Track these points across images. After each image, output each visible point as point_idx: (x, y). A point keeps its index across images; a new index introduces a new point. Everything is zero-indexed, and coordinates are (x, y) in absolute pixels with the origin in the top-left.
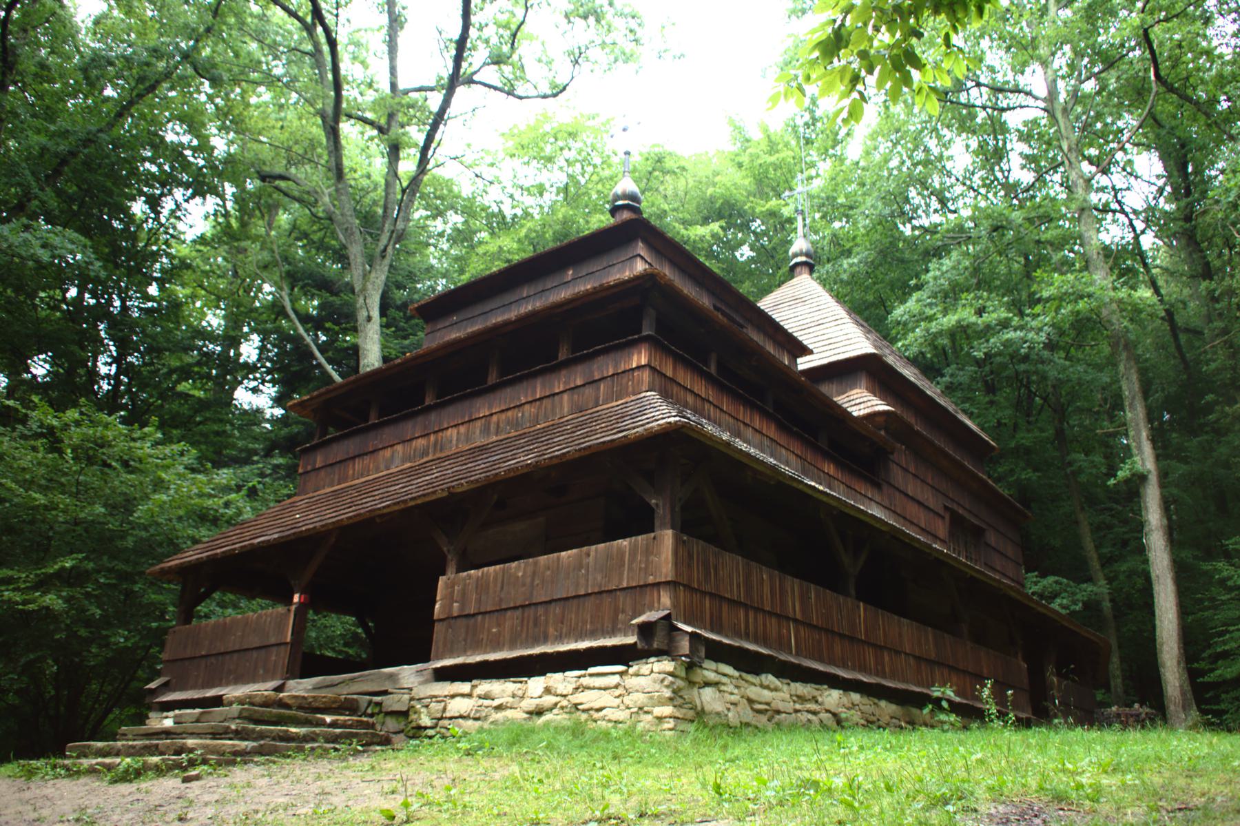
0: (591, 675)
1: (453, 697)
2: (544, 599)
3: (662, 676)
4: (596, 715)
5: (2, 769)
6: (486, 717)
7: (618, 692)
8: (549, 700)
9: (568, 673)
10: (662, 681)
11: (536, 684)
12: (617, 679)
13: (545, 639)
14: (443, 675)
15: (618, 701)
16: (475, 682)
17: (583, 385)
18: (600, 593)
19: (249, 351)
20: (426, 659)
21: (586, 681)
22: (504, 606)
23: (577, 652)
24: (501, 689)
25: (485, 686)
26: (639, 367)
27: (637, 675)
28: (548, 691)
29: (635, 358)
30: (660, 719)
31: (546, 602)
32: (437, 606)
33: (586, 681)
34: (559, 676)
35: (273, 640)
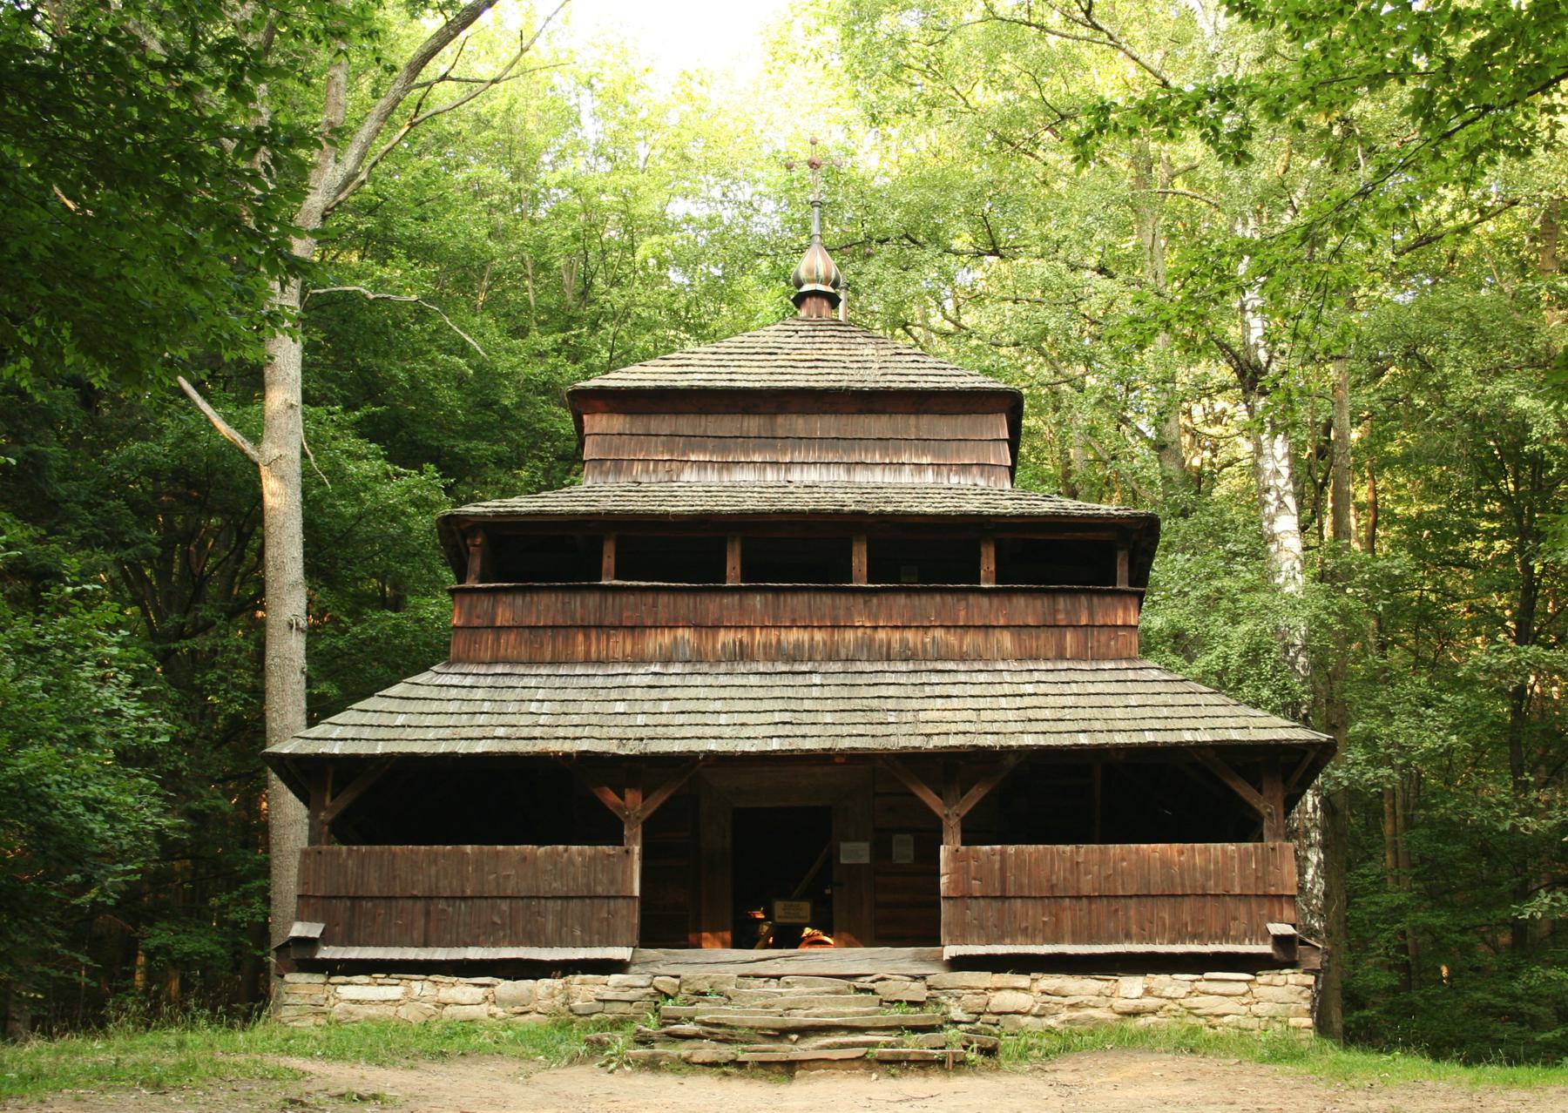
0: (475, 985)
3: (1300, 988)
4: (1216, 1021)
5: (8, 1053)
7: (1245, 1000)
8: (1150, 1002)
10: (1300, 993)
11: (1131, 987)
12: (1243, 987)
14: (959, 964)
15: (1245, 1008)
16: (1033, 975)
20: (935, 941)
21: (1202, 986)
23: (995, 956)
25: (1161, 981)
29: (1120, 613)
32: (943, 880)
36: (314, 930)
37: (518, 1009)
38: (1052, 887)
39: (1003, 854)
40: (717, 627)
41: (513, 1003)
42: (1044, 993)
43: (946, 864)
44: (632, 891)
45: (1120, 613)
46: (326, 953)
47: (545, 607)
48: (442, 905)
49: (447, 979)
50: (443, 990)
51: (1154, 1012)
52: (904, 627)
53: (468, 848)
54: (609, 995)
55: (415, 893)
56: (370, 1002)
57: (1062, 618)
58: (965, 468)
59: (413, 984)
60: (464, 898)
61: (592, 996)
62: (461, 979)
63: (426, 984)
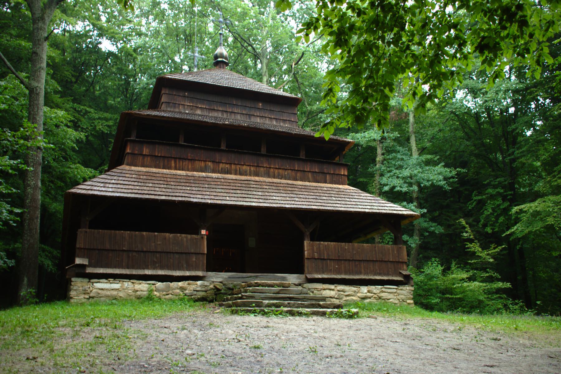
1: (324, 289)
2: (358, 259)
6: (342, 298)
8: (369, 295)
9: (377, 286)
11: (364, 290)
12: (395, 290)
13: (360, 273)
16: (335, 285)
17: (319, 173)
18: (382, 261)
19: (358, 113)
21: (384, 290)
22: (341, 258)
24: (349, 289)
25: (372, 288)
26: (344, 175)
27: (402, 290)
28: (369, 292)
29: (342, 171)
30: (409, 304)
31: (359, 260)
32: (306, 253)
33: (384, 290)
34: (373, 287)
35: (192, 251)
36: (85, 262)
37: (164, 293)
38: (339, 256)
39: (186, 237)
40: (219, 163)
41: (163, 291)
42: (338, 291)
43: (307, 247)
44: (204, 251)
45: (342, 171)
46: (89, 270)
47: (160, 151)
48: (134, 254)
49: (138, 282)
50: (136, 285)
51: (370, 298)
52: (279, 169)
53: (144, 233)
54: (199, 289)
55: (124, 248)
56: (107, 289)
57: (325, 171)
58: (284, 121)
59: (125, 283)
60: (143, 252)
61: (192, 289)
62: (143, 282)
63: (129, 283)
